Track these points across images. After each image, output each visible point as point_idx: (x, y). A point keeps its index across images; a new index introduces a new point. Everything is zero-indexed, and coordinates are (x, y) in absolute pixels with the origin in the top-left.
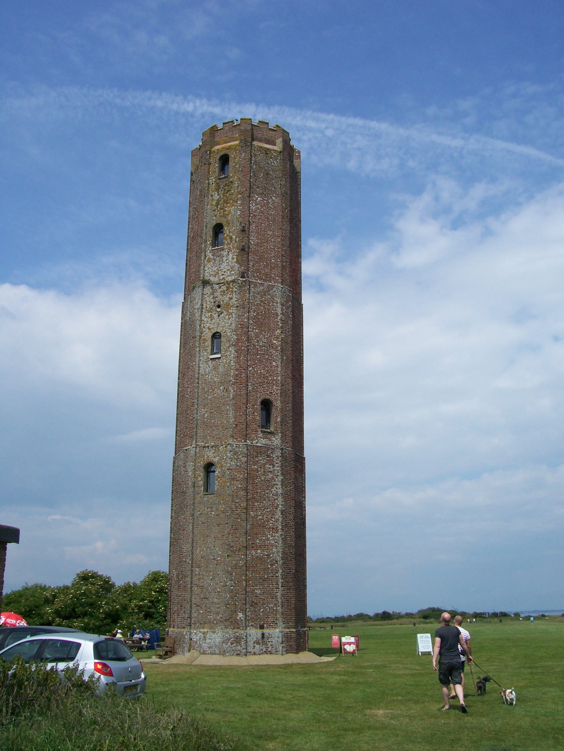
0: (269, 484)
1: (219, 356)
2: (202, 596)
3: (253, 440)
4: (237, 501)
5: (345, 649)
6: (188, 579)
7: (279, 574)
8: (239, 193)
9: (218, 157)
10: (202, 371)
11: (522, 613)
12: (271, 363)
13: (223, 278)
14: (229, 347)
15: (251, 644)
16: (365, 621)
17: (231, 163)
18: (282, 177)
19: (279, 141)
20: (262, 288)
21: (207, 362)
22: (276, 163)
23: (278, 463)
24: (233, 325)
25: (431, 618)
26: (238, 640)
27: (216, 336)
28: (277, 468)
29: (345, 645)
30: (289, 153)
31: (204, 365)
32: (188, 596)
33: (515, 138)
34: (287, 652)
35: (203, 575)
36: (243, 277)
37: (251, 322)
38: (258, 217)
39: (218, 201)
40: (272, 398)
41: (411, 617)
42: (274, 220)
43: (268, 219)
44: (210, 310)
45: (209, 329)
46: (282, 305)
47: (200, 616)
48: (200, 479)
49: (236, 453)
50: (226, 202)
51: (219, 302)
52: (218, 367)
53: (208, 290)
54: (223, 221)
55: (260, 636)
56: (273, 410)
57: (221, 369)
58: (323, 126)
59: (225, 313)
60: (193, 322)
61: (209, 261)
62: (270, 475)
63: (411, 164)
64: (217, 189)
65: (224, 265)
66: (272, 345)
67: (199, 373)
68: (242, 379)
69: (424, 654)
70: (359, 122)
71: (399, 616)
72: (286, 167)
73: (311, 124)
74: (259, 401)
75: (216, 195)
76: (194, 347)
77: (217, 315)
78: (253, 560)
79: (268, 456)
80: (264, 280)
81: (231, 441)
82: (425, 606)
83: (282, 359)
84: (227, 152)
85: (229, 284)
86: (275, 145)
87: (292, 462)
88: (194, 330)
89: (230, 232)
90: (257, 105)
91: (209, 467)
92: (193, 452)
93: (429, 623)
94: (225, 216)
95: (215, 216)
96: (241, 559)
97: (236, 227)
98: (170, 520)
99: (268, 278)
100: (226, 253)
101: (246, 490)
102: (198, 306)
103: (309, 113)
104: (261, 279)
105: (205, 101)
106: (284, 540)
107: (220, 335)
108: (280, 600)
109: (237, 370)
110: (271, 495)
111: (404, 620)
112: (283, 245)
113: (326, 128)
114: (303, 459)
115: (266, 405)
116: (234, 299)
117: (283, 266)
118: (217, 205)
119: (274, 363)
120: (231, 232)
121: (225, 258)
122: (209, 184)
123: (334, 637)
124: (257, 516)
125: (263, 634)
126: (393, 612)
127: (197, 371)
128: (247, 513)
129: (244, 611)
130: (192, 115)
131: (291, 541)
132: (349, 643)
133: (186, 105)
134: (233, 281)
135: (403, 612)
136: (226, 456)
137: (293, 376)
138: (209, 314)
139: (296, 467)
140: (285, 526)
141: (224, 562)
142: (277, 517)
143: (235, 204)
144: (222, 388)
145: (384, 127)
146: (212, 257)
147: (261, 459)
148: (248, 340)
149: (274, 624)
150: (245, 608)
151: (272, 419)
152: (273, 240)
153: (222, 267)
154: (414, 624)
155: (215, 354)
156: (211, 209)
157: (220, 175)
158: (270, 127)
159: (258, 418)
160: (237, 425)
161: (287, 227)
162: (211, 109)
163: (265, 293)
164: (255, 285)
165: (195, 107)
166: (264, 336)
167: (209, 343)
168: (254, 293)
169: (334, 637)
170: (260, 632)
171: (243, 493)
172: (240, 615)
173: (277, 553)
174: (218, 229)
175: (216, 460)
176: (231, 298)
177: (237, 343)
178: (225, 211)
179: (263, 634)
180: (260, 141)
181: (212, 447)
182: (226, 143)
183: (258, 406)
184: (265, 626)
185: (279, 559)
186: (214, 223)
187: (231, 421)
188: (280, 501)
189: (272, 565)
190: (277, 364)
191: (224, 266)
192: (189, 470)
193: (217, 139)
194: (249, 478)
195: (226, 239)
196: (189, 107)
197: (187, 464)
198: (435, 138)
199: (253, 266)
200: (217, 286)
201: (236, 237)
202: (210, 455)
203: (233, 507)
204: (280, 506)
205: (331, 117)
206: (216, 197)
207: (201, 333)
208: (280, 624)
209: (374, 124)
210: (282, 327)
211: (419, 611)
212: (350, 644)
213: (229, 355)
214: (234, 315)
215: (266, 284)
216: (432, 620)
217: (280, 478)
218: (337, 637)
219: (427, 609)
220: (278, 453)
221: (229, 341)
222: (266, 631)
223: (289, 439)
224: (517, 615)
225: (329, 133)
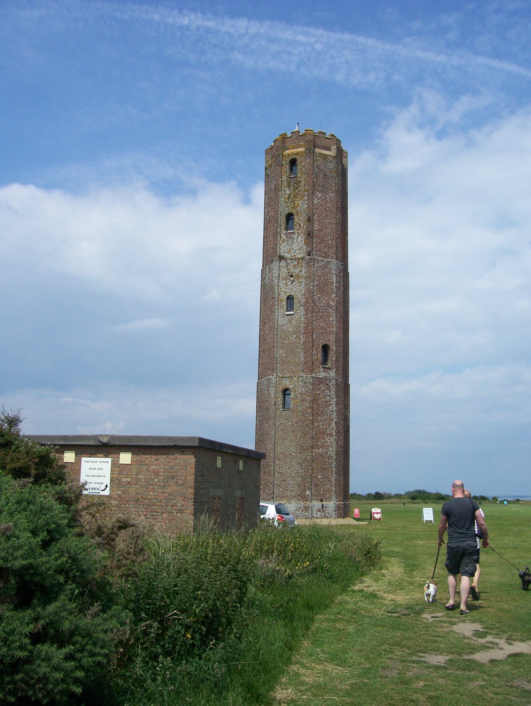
0: (327, 404)
1: (292, 313)
2: (282, 479)
3: (316, 373)
4: (306, 415)
5: (374, 517)
6: (272, 468)
8: (305, 191)
10: (280, 323)
11: (500, 497)
12: (329, 319)
13: (295, 255)
14: (300, 307)
15: (315, 512)
16: (360, 500)
17: (299, 167)
18: (336, 177)
19: (334, 148)
21: (283, 317)
22: (331, 166)
23: (333, 389)
24: (303, 291)
25: (418, 499)
26: (306, 509)
27: (290, 298)
28: (333, 393)
29: (374, 513)
30: (341, 154)
31: (281, 318)
32: (271, 479)
33: (496, 54)
34: (338, 517)
35: (282, 465)
37: (315, 289)
38: (319, 209)
39: (289, 195)
40: (330, 344)
41: (400, 498)
42: (330, 211)
43: (326, 210)
44: (285, 279)
45: (284, 292)
46: (337, 276)
47: (280, 493)
48: (279, 399)
49: (305, 383)
50: (295, 196)
51: (292, 273)
53: (283, 263)
54: (294, 211)
55: (320, 506)
56: (330, 352)
57: (294, 323)
58: (313, 40)
59: (296, 281)
60: (272, 287)
61: (283, 241)
62: (328, 398)
63: (396, 77)
64: (289, 186)
65: (294, 246)
66: (329, 305)
67: (278, 325)
68: (309, 330)
69: (115, 481)
70: (346, 37)
71: (389, 497)
72: (339, 169)
73: (301, 38)
74: (321, 345)
75: (288, 191)
76: (274, 305)
77: (290, 282)
79: (327, 385)
80: (324, 257)
81: (302, 374)
82: (412, 488)
84: (296, 157)
85: (299, 260)
86: (330, 150)
88: (274, 292)
89: (299, 220)
90: (250, 19)
91: (285, 392)
92: (274, 381)
93: (417, 503)
94: (294, 208)
95: (288, 207)
96: (309, 455)
98: (255, 427)
99: (326, 255)
100: (296, 236)
101: (312, 408)
102: (277, 275)
103: (299, 28)
104: (321, 257)
105: (199, 15)
107: (293, 297)
108: (334, 483)
109: (306, 324)
111: (393, 500)
112: (337, 230)
113: (316, 42)
114: (349, 385)
115: (325, 348)
116: (303, 272)
117: (337, 246)
118: (289, 198)
119: (331, 319)
120: (300, 220)
121: (295, 240)
122: (282, 181)
123: (355, 510)
125: (323, 505)
126: (384, 493)
127: (276, 323)
128: (313, 424)
129: (310, 490)
130: (188, 29)
131: (341, 443)
132: (377, 512)
133: (181, 19)
134: (302, 258)
135: (393, 494)
136: (299, 385)
137: (343, 326)
138: (285, 281)
139: (345, 392)
140: (338, 433)
141: (297, 456)
142: (332, 426)
143: (303, 199)
144: (295, 336)
145: (370, 42)
146: (286, 239)
147: (322, 387)
148: (313, 302)
149: (329, 499)
150: (309, 488)
153: (293, 247)
154: (404, 504)
155: (289, 311)
156: (284, 201)
157: (290, 175)
158: (327, 136)
159: (320, 358)
160: (306, 363)
161: (339, 216)
162: (205, 23)
163: (324, 267)
165: (190, 20)
166: (324, 299)
167: (284, 303)
168: (317, 267)
169: (355, 510)
170: (320, 503)
171: (310, 410)
172: (308, 492)
173: (332, 451)
174: (289, 217)
175: (291, 387)
176: (301, 271)
177: (306, 304)
178: (294, 204)
179: (323, 505)
180: (320, 148)
181: (288, 377)
182: (293, 148)
183: (320, 350)
184: (324, 499)
186: (287, 212)
187: (302, 360)
189: (329, 459)
190: (333, 318)
191: (295, 246)
193: (287, 145)
194: (315, 400)
195: (296, 226)
196: (185, 21)
197: (270, 389)
198: (421, 54)
199: (316, 247)
200: (290, 261)
202: (287, 383)
203: (304, 419)
204: (335, 419)
205: (320, 32)
206: (288, 192)
207: (279, 295)
208: (334, 498)
209: (361, 39)
211: (406, 493)
212: (377, 513)
213: (300, 312)
215: (325, 260)
216: (420, 500)
217: (335, 400)
218: (358, 510)
219: (414, 491)
220: (333, 382)
221: (300, 302)
222: (325, 503)
223: (340, 372)
224: (495, 499)
225: (319, 47)
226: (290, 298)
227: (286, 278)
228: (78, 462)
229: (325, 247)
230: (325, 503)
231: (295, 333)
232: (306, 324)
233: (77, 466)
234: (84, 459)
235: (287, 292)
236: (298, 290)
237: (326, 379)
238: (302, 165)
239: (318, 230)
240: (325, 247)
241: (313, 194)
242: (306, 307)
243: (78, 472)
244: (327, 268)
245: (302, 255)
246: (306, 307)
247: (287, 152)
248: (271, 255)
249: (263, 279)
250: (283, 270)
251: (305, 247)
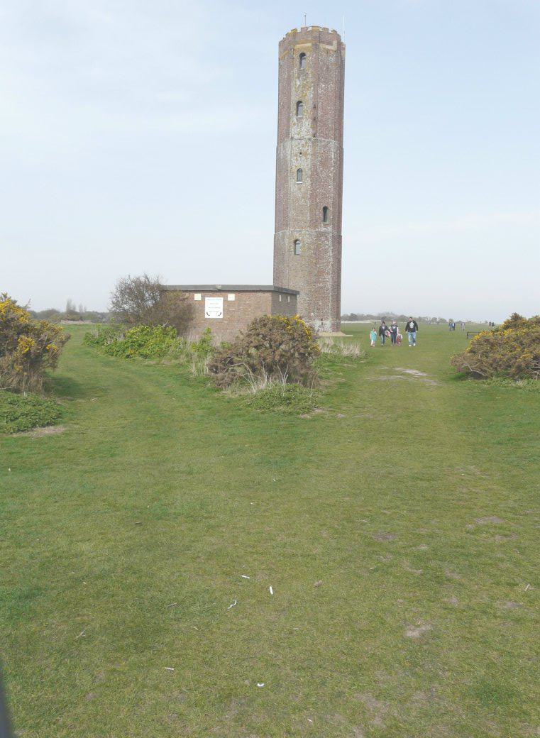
0: (326, 251)
19: (335, 43)
22: (332, 59)
23: (330, 240)
27: (299, 171)
30: (341, 46)
31: (293, 186)
44: (296, 155)
52: (298, 189)
57: (302, 190)
61: (295, 124)
65: (302, 129)
68: (313, 197)
69: (226, 310)
76: (287, 176)
84: (305, 51)
97: (310, 104)
99: (327, 136)
112: (335, 116)
115: (325, 209)
134: (310, 139)
136: (306, 236)
140: (333, 271)
151: (328, 216)
163: (325, 147)
167: (295, 174)
173: (329, 285)
183: (321, 211)
193: (297, 40)
194: (317, 248)
202: (297, 236)
206: (298, 83)
215: (327, 140)
217: (332, 248)
220: (331, 235)
222: (324, 322)
228: (203, 300)
230: (324, 322)
231: (304, 198)
233: (202, 303)
234: (206, 299)
238: (310, 57)
239: (322, 116)
243: (203, 306)
245: (309, 137)
247: (298, 46)
248: (284, 134)
249: (278, 154)
251: (311, 130)
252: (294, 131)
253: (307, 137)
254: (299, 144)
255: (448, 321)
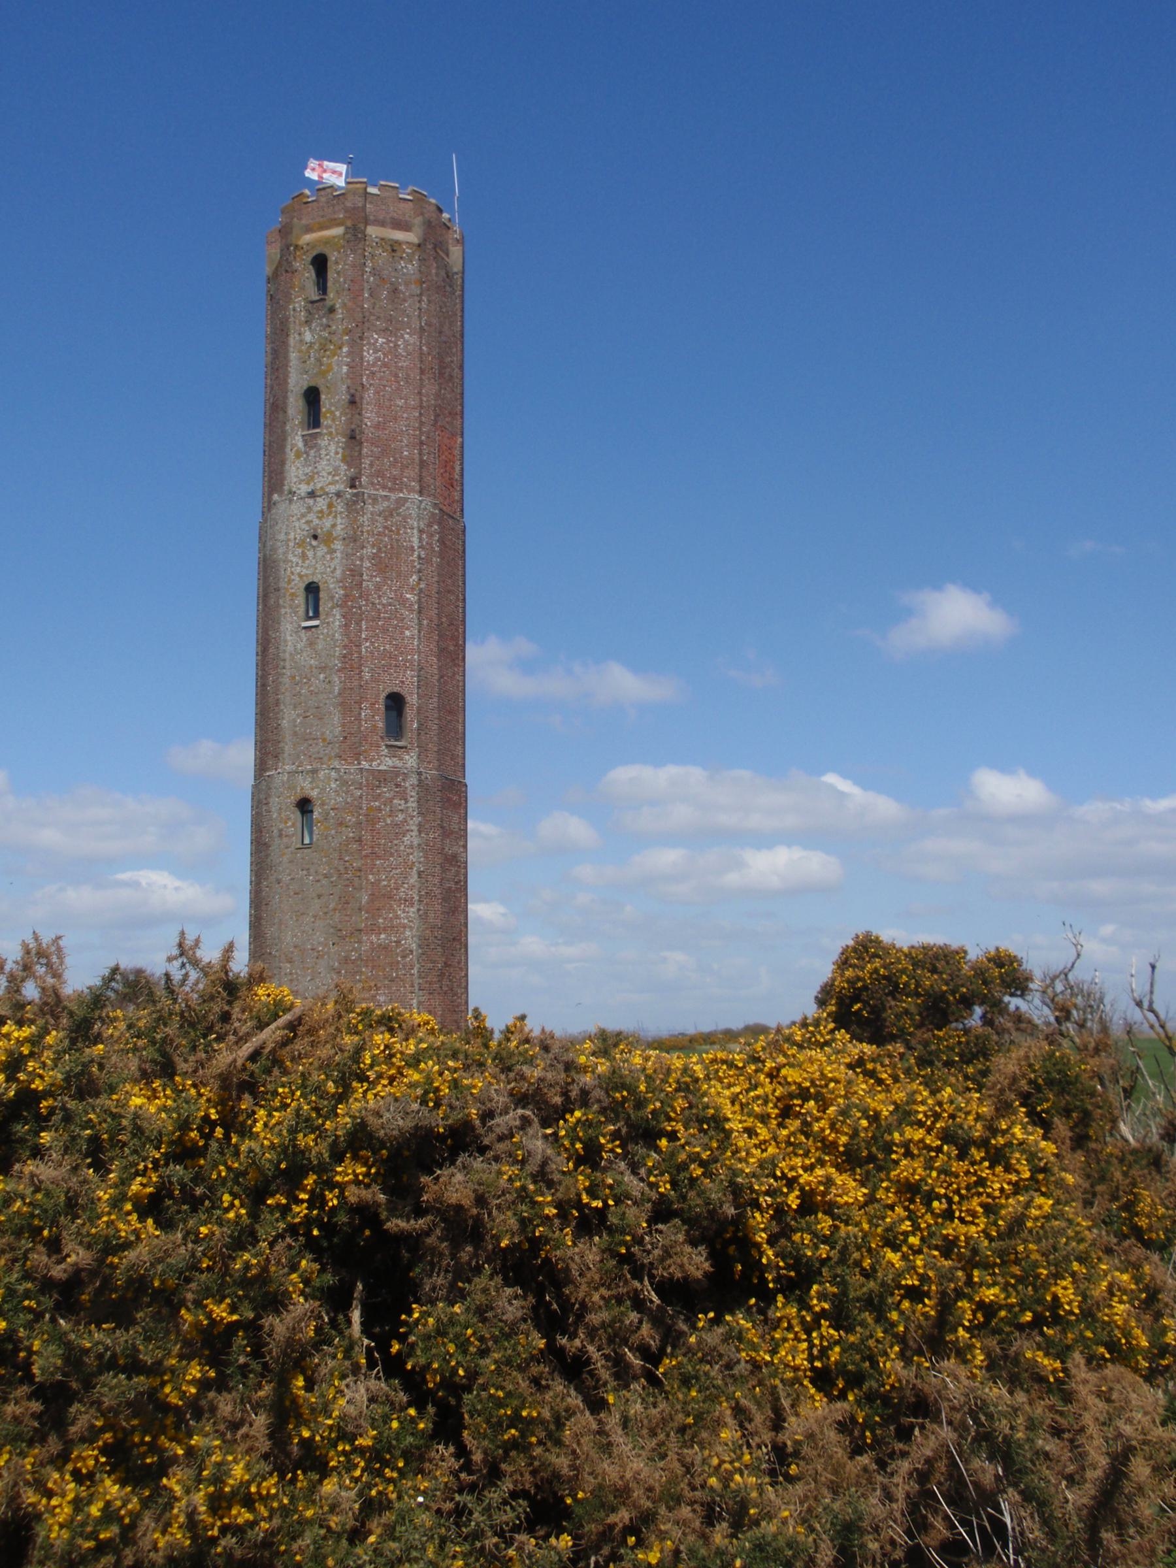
0: (399, 830)
3: (372, 760)
7: (415, 971)
9: (310, 259)
12: (402, 633)
14: (332, 608)
20: (386, 504)
28: (412, 804)
36: (353, 486)
43: (396, 376)
46: (421, 531)
49: (344, 783)
51: (315, 530)
61: (298, 456)
62: (401, 817)
66: (403, 602)
68: (351, 664)
74: (383, 695)
78: (373, 949)
79: (397, 786)
80: (391, 490)
83: (420, 624)
84: (326, 251)
87: (439, 793)
94: (323, 374)
96: (354, 949)
99: (396, 484)
101: (360, 840)
104: (384, 487)
106: (423, 917)
109: (345, 647)
110: (402, 848)
112: (422, 423)
115: (395, 702)
116: (339, 528)
119: (407, 633)
121: (323, 452)
124: (380, 880)
134: (338, 495)
142: (412, 881)
144: (322, 676)
147: (386, 791)
152: (405, 415)
159: (381, 725)
160: (345, 738)
163: (389, 514)
164: (375, 500)
168: (372, 514)
175: (314, 794)
180: (382, 224)
181: (308, 772)
185: (414, 946)
188: (416, 857)
192: (273, 809)
199: (371, 465)
201: (341, 414)
202: (306, 786)
203: (341, 868)
210: (420, 571)
214: (339, 555)
215: (393, 496)
217: (417, 820)
220: (413, 780)
226: (312, 590)
227: (303, 541)
229: (393, 465)
231: (322, 669)
232: (345, 647)
235: (306, 575)
236: (327, 566)
237: (395, 773)
239: (377, 426)
240: (393, 465)
241: (361, 338)
242: (345, 610)
244: (398, 515)
245: (340, 487)
246: (345, 610)
250: (297, 524)
251: (344, 467)
252: (295, 472)
253: (332, 489)
254: (309, 509)
255: (86, 991)
